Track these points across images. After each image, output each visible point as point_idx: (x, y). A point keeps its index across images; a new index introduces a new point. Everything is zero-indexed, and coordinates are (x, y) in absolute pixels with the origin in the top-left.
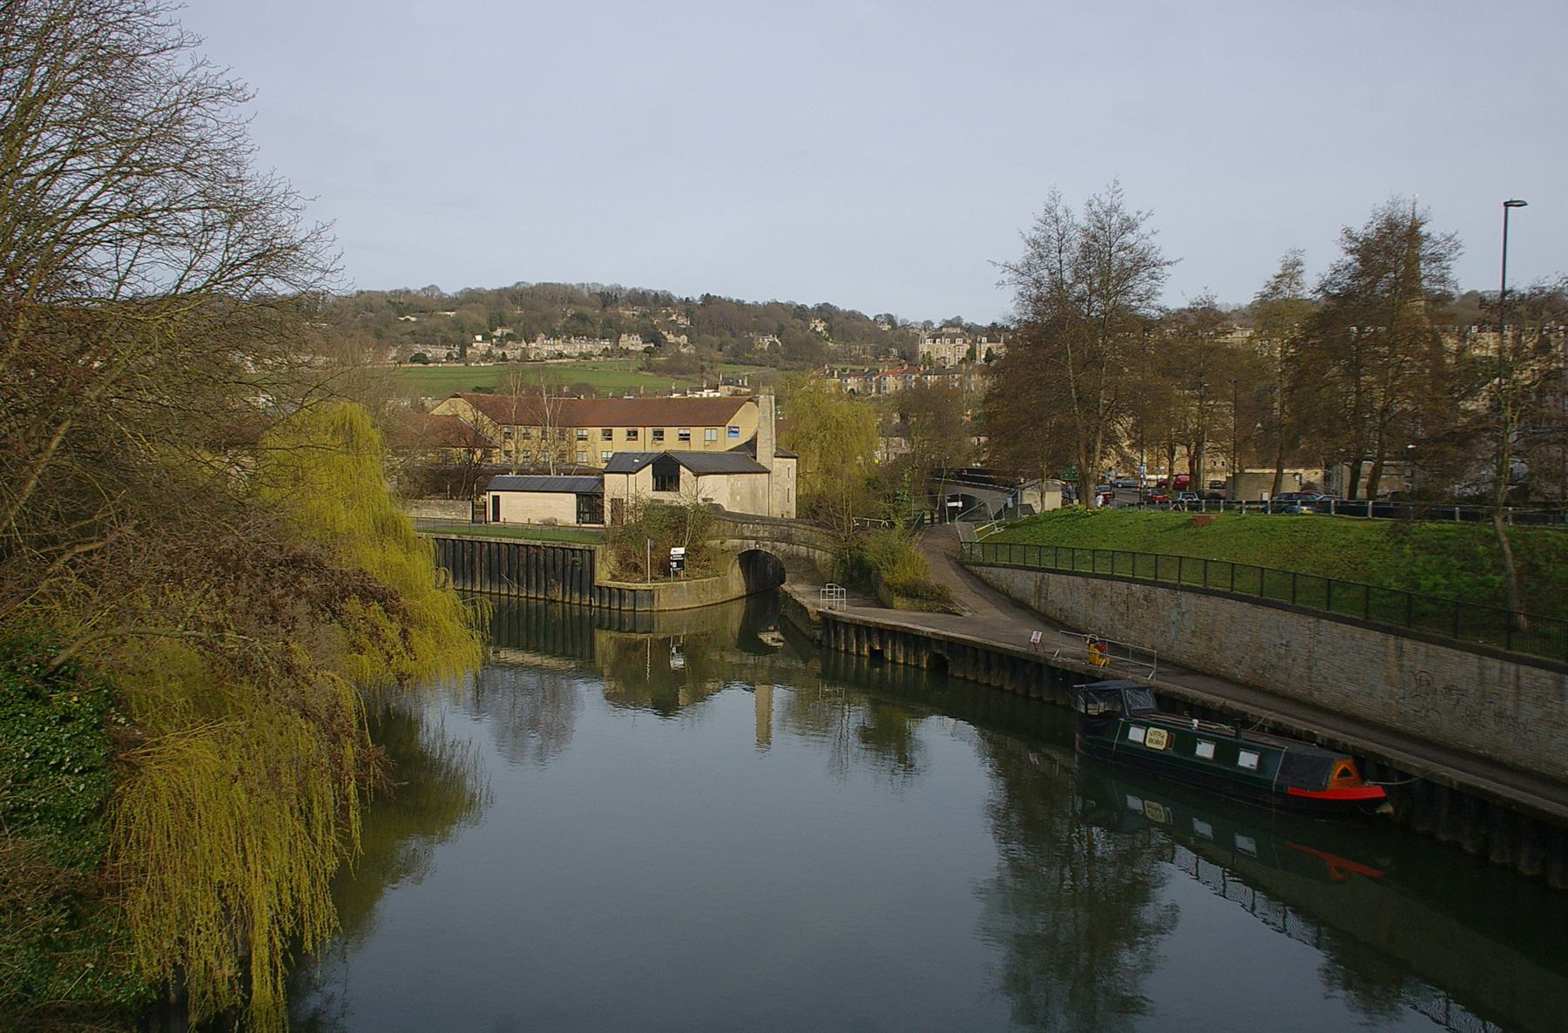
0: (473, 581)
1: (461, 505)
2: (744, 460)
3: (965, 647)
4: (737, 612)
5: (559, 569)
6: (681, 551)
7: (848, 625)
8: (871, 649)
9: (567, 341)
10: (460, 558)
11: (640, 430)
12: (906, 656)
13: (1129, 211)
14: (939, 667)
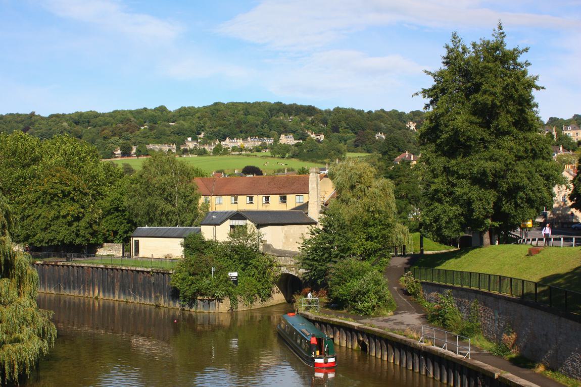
9: (245, 139)
11: (255, 197)
13: (509, 45)
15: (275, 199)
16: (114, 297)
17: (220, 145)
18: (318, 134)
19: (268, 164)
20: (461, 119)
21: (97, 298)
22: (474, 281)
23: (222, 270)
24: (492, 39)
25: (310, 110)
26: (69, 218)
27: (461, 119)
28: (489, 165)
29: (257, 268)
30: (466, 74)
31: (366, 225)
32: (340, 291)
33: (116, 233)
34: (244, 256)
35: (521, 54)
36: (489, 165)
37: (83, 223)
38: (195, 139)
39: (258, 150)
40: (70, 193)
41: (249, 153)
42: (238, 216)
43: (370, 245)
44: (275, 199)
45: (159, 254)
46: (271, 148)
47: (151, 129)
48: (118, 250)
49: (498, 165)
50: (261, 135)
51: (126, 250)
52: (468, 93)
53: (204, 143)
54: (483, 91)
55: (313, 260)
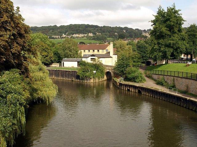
0: (59, 77)
1: (57, 64)
2: (108, 55)
3: (144, 88)
4: (105, 83)
5: (74, 75)
6: (94, 72)
7: (123, 85)
8: (128, 89)
9: (79, 34)
10: (53, 73)
11: (90, 50)
12: (134, 90)
13: (177, 9)
14: (139, 92)
15: (96, 51)
16: (59, 78)
17: (72, 36)
18: (99, 33)
19: (101, 42)
20: (164, 29)
21: (54, 79)
22: (163, 72)
23: (91, 71)
24: (172, 7)
25: (97, 27)
26: (45, 56)
27: (164, 29)
28: (172, 42)
29: (101, 70)
30: (163, 16)
31: (133, 58)
32: (130, 76)
33: (55, 60)
34: (98, 67)
35: (19, 11)
36: (172, 42)
37: (48, 58)
38: (65, 34)
39: (83, 37)
40: (45, 49)
41: (80, 38)
42: (93, 55)
43: (134, 64)
44: (91, 51)
45: (70, 66)
46: (86, 37)
47: (53, 31)
48: (58, 65)
49: (174, 42)
50: (84, 33)
51: (60, 65)
52: (165, 22)
53: (67, 35)
54: (168, 21)
55: (119, 68)
